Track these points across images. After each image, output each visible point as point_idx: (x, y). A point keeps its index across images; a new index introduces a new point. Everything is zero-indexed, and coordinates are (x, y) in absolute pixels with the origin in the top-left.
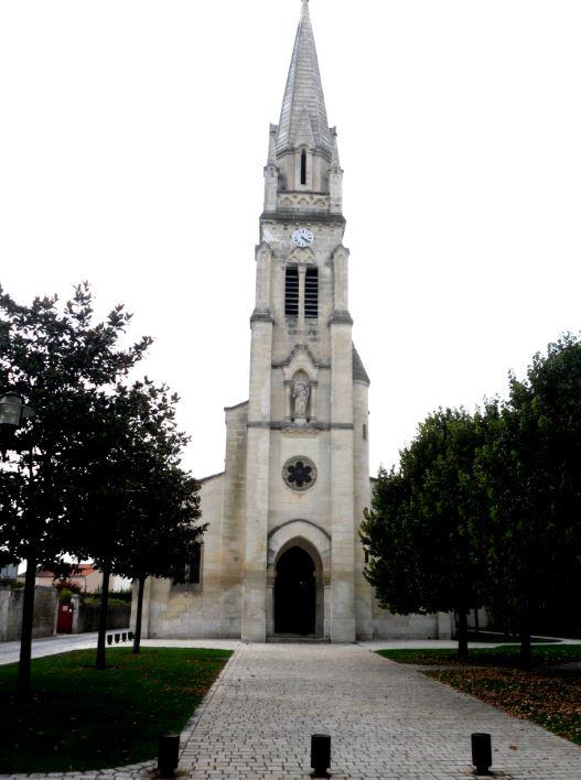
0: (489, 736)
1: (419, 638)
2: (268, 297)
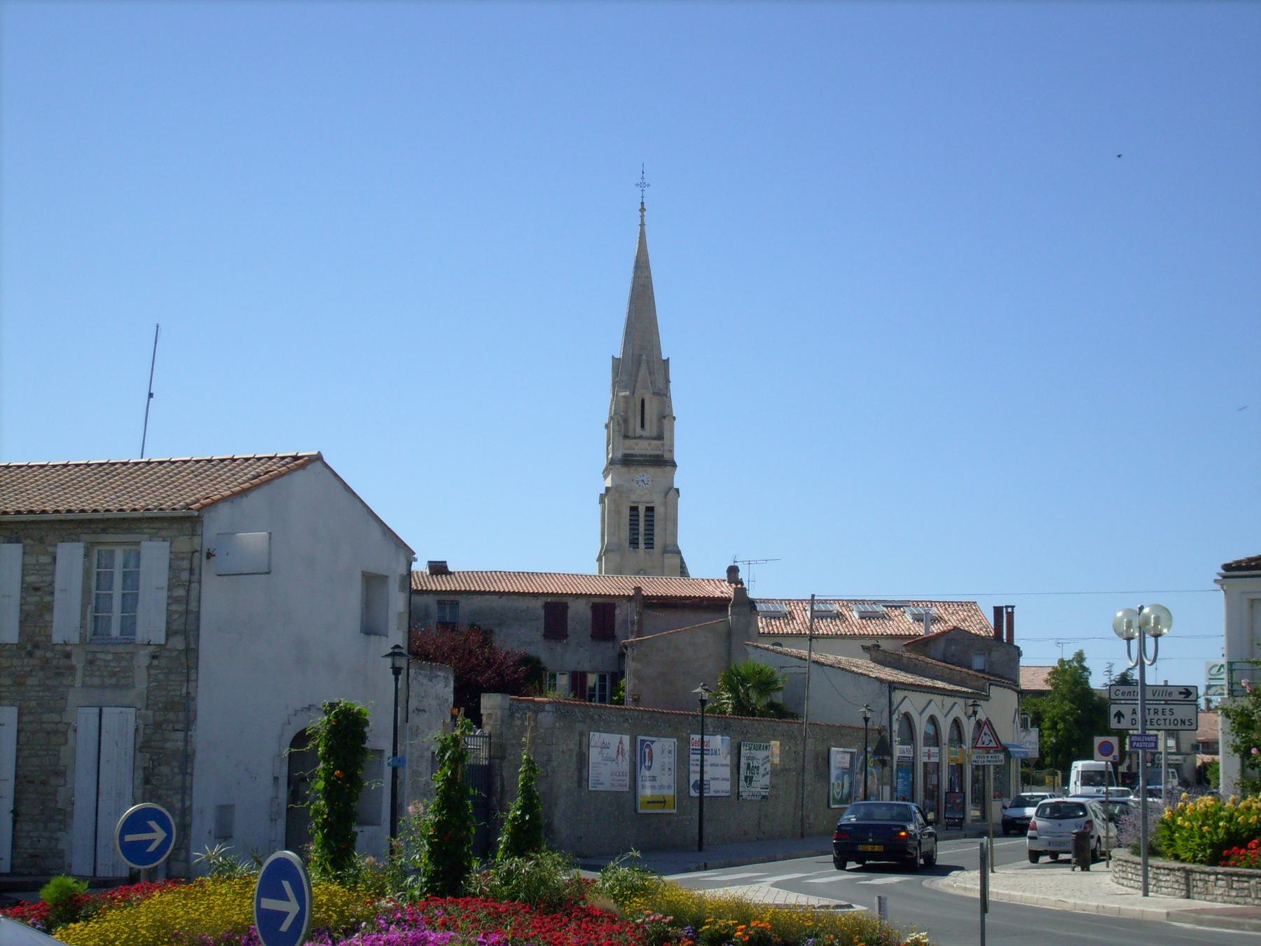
0: (1119, 711)
1: (888, 820)
2: (801, 760)
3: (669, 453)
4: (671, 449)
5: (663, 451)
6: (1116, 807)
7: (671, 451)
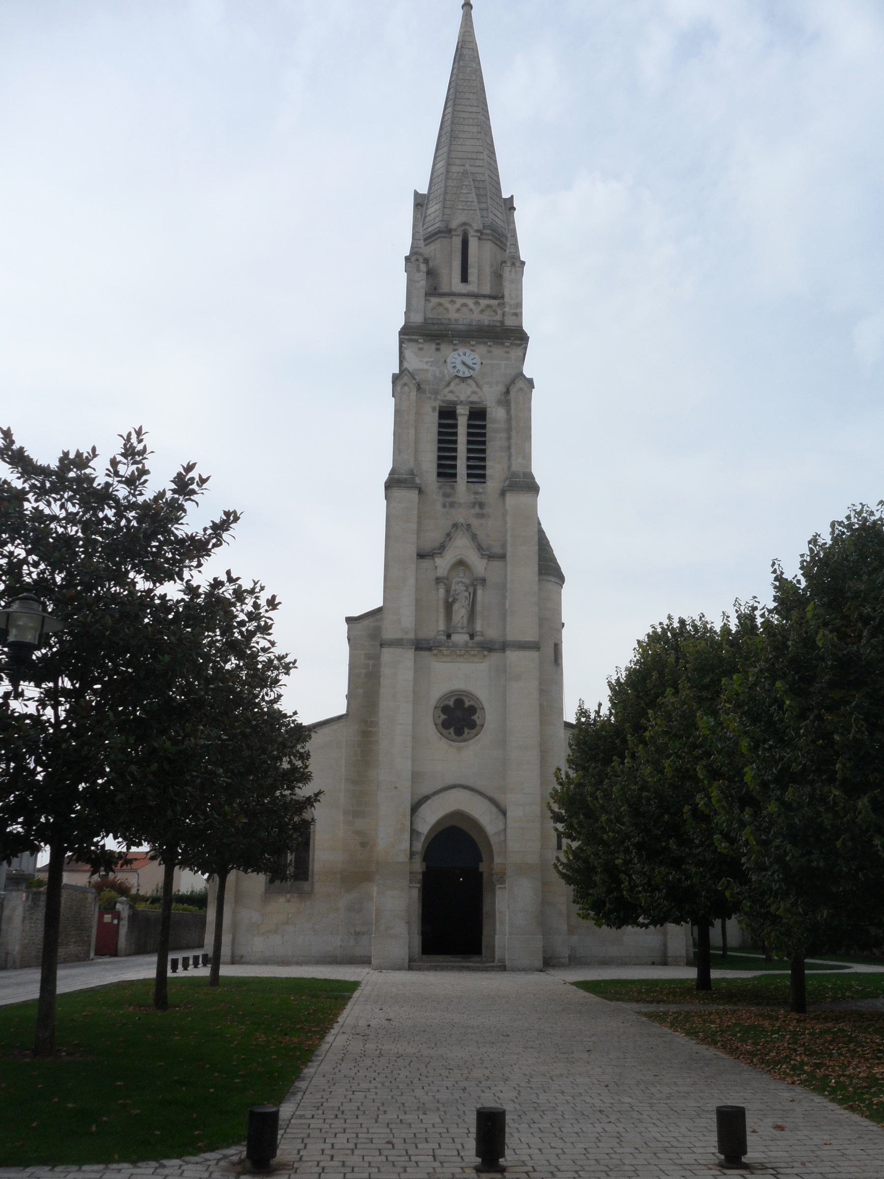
3: (515, 317)
4: (518, 311)
5: (504, 314)
6: (807, 963)
7: (518, 315)
